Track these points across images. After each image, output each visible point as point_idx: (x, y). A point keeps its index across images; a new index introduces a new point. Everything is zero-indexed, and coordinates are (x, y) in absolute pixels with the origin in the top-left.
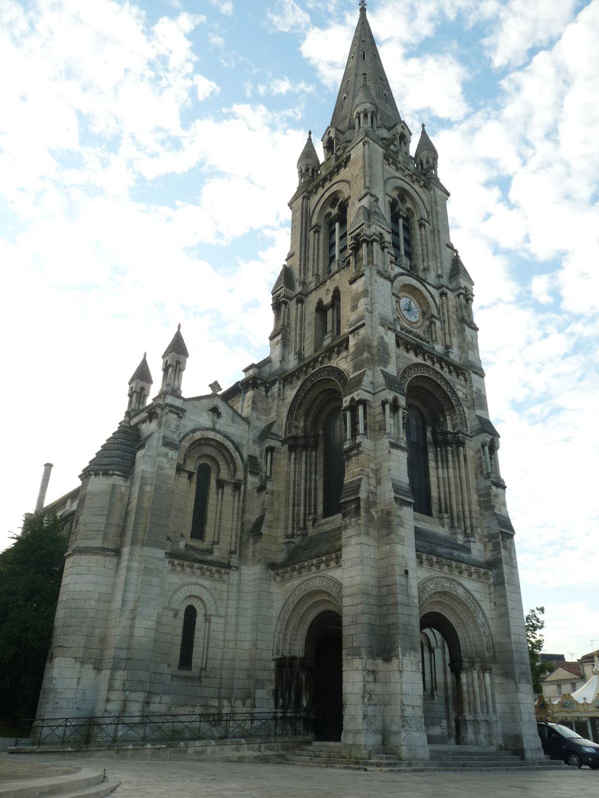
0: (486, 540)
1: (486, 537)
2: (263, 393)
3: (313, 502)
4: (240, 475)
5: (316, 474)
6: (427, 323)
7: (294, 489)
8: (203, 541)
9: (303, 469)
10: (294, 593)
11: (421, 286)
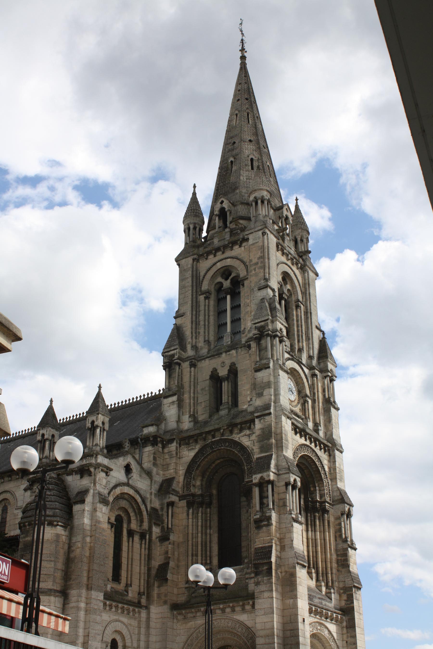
0: (342, 591)
1: (341, 589)
2: (160, 449)
3: (208, 553)
4: (146, 525)
5: (210, 529)
6: (302, 401)
7: (192, 541)
8: (120, 583)
9: (200, 524)
10: (198, 630)
11: (299, 368)
